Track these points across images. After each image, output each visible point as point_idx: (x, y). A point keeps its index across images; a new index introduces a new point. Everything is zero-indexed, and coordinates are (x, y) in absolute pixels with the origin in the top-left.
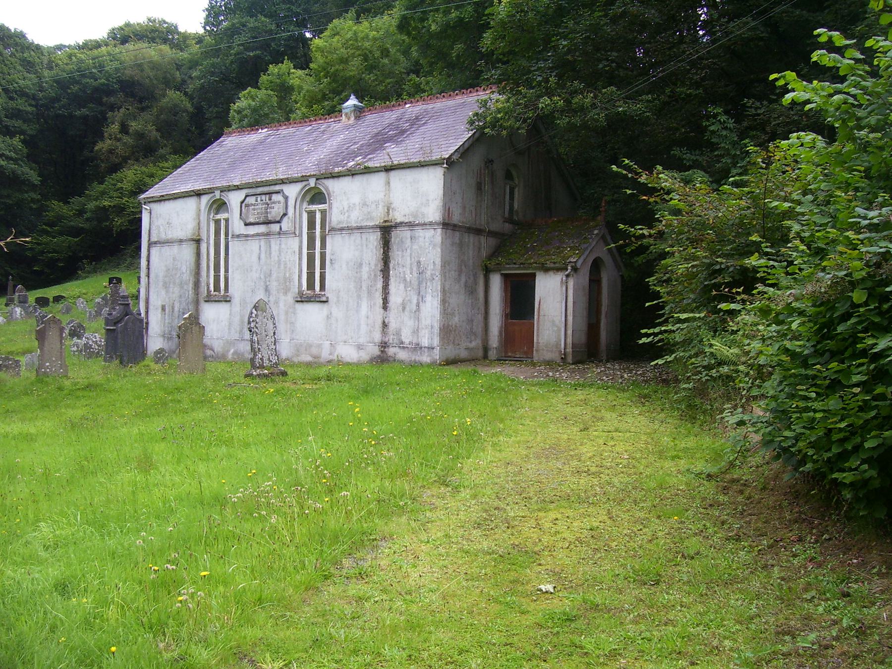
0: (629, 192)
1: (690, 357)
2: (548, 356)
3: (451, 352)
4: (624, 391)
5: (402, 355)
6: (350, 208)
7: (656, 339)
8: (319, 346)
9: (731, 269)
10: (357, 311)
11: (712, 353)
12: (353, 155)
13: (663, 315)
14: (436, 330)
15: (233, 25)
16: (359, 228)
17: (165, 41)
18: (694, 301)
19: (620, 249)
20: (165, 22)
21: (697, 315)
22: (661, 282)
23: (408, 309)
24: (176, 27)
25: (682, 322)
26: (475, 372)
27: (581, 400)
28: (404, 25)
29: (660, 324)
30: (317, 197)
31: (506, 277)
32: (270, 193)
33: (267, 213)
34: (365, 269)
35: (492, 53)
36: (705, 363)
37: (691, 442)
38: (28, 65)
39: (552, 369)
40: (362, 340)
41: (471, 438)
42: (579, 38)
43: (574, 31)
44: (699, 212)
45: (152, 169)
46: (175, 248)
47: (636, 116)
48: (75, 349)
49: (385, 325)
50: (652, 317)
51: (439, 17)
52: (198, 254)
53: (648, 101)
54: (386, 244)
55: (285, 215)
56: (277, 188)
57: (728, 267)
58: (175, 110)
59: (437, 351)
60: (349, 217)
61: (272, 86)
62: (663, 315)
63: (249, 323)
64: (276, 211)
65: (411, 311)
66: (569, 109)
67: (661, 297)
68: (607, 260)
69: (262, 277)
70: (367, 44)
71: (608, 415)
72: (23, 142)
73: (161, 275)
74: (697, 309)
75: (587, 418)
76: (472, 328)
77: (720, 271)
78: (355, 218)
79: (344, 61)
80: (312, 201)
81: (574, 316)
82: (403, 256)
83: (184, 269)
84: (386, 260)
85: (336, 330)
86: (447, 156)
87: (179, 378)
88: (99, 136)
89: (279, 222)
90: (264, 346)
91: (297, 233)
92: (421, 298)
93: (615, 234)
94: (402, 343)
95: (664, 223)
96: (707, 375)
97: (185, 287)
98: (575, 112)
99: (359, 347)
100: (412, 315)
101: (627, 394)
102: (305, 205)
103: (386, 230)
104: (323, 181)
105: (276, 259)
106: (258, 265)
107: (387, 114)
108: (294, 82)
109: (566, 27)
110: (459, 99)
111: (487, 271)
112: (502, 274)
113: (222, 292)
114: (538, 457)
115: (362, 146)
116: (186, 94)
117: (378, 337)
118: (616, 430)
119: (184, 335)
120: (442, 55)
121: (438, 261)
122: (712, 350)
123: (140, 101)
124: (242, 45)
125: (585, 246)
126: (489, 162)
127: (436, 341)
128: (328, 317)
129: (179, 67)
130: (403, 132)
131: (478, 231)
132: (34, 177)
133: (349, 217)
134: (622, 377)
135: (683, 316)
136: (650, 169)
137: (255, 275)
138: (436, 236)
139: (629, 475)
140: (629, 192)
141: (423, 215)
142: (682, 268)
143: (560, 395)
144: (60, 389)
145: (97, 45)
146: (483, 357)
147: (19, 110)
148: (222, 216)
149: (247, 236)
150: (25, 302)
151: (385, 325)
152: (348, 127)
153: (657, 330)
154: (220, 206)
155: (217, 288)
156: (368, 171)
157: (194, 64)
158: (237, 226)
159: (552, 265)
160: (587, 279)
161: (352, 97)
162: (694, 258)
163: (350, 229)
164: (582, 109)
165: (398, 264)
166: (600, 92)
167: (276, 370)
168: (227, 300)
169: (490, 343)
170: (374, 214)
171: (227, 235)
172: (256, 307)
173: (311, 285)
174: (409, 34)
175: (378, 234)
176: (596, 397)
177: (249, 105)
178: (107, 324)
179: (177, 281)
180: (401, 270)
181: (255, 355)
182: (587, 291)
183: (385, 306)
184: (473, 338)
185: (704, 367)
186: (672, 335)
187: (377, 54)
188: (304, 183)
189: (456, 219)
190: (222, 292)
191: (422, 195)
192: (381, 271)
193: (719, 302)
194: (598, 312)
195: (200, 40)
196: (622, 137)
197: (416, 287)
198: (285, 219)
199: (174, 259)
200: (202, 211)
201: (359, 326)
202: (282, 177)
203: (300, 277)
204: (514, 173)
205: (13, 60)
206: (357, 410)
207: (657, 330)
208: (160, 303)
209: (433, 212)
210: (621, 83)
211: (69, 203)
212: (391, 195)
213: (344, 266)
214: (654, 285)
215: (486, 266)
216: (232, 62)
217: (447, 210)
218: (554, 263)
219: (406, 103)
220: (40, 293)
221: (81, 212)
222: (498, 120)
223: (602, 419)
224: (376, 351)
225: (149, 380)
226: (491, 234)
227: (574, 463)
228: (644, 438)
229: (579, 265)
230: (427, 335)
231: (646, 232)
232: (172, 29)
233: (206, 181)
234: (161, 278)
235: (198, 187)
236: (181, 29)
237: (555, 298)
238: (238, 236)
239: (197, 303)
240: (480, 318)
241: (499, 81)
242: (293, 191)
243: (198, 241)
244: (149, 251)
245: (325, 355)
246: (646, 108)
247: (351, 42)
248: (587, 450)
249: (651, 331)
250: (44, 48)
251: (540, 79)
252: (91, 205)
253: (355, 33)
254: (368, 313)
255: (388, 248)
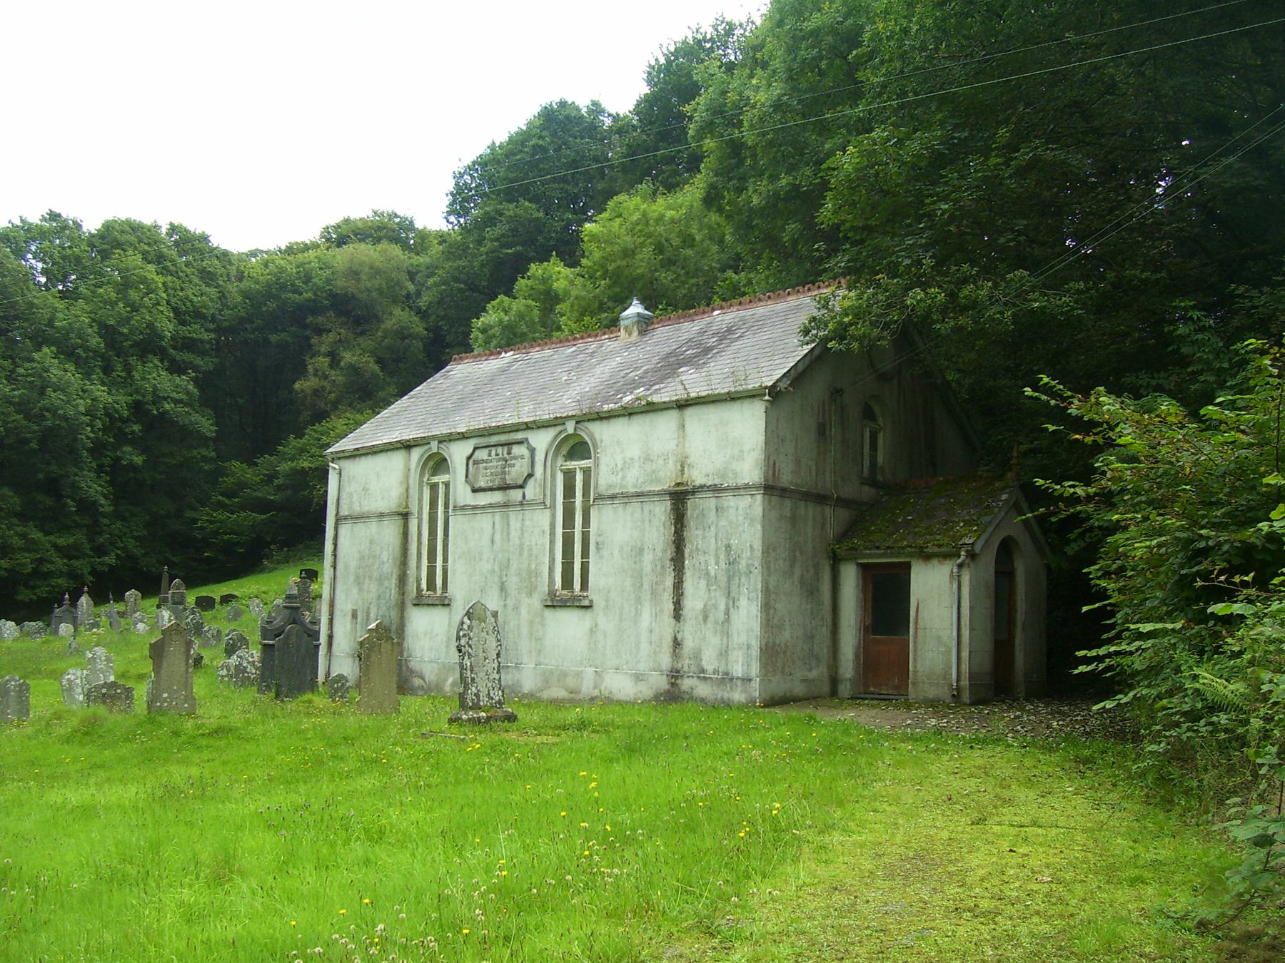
0: (1051, 428)
1: (1159, 697)
2: (932, 692)
3: (780, 686)
4: (1051, 750)
5: (703, 690)
6: (626, 465)
7: (1101, 666)
8: (578, 675)
9: (1226, 548)
10: (636, 619)
11: (1197, 690)
12: (633, 385)
13: (1113, 626)
14: (755, 652)
15: (486, 213)
16: (638, 495)
17: (396, 240)
18: (1163, 602)
19: (1041, 520)
20: (396, 216)
21: (1170, 626)
22: (1106, 574)
23: (711, 618)
24: (411, 223)
25: (1144, 637)
26: (811, 718)
27: (979, 768)
28: (711, 199)
29: (1109, 642)
30: (578, 448)
31: (865, 568)
32: (509, 444)
33: (504, 473)
34: (648, 558)
35: (836, 227)
36: (1186, 708)
37: (1164, 850)
38: (208, 277)
39: (935, 714)
40: (643, 667)
41: (777, 840)
42: (967, 197)
43: (957, 189)
44: (1168, 457)
45: (358, 416)
46: (373, 527)
47: (1062, 314)
48: (224, 672)
49: (677, 644)
50: (1096, 629)
51: (763, 185)
52: (405, 534)
53: (1079, 292)
54: (679, 519)
55: (530, 476)
56: (520, 436)
57: (1219, 545)
58: (403, 334)
59: (756, 684)
60: (623, 478)
61: (533, 294)
62: (1113, 626)
63: (458, 638)
64: (517, 470)
65: (716, 622)
66: (953, 305)
67: (1110, 597)
68: (1023, 539)
69: (497, 569)
70: (661, 229)
71: (1022, 794)
72: (196, 381)
73: (353, 564)
74: (1169, 616)
75: (986, 799)
76: (811, 650)
77: (1205, 552)
78: (633, 480)
79: (628, 253)
80: (571, 456)
81: (971, 629)
82: (704, 538)
83: (385, 556)
84: (679, 543)
85: (605, 649)
86: (770, 384)
87: (352, 721)
88: (301, 371)
89: (521, 487)
90: (482, 674)
91: (548, 503)
92: (732, 601)
93: (1036, 497)
94: (703, 671)
95: (1109, 475)
96: (1189, 729)
97: (386, 584)
98: (964, 309)
99: (638, 678)
100: (719, 628)
101: (1055, 757)
102: (560, 461)
103: (680, 498)
104: (586, 424)
105: (517, 541)
106: (491, 552)
107: (686, 326)
108: (560, 285)
109: (946, 183)
110: (793, 301)
111: (835, 561)
112: (859, 565)
113: (439, 592)
114: (890, 877)
115: (646, 372)
116: (419, 312)
117: (666, 661)
118: (1034, 824)
119: (368, 657)
120: (771, 241)
121: (758, 545)
122: (1197, 685)
123: (358, 321)
124: (497, 240)
125: (988, 518)
126: (836, 392)
127: (755, 670)
128: (593, 631)
129: (412, 276)
130: (707, 350)
131: (820, 499)
132: (205, 424)
133: (623, 478)
134: (1049, 727)
135: (1146, 628)
136: (1086, 393)
137: (486, 566)
138: (756, 504)
139: (1048, 919)
140: (1051, 428)
141: (735, 474)
142: (1140, 548)
143: (946, 758)
144: (176, 734)
145: (306, 248)
146: (828, 693)
147: (193, 340)
148: (440, 479)
149: (475, 507)
150: (182, 602)
151: (677, 644)
152: (628, 347)
153: (1102, 651)
154: (438, 464)
155: (431, 585)
156: (652, 408)
157: (431, 270)
158: (462, 494)
159: (936, 550)
160: (993, 570)
161: (635, 302)
162: (1161, 531)
163: (626, 497)
164: (974, 305)
165: (697, 549)
166: (1004, 279)
167: (500, 713)
168: (445, 603)
169: (841, 671)
170: (662, 474)
171: (446, 506)
172: (468, 614)
173: (567, 582)
174: (720, 210)
175: (667, 504)
176: (1005, 760)
177: (501, 321)
178: (264, 637)
179: (375, 574)
180: (702, 559)
181: (466, 688)
182: (992, 588)
183: (677, 614)
184: (814, 663)
185: (1184, 714)
186: (1126, 661)
187: (676, 241)
188: (559, 428)
189: (786, 479)
190: (439, 592)
191: (733, 445)
192: (672, 559)
193: (1208, 604)
194: (1011, 622)
195: (442, 238)
196: (1036, 342)
197: (723, 584)
198: (531, 483)
199: (372, 542)
200: (412, 471)
201: (638, 644)
202: (526, 420)
203: (551, 569)
204: (877, 409)
205: (189, 271)
206: (593, 784)
207: (1102, 651)
208: (349, 607)
209: (750, 470)
210: (1033, 265)
211: (256, 464)
212: (687, 445)
213: (616, 553)
214: (1099, 578)
215: (834, 552)
216: (482, 265)
217: (771, 465)
218: (940, 546)
219: (713, 310)
220: (204, 592)
221: (270, 478)
222: (845, 328)
223: (1009, 802)
224: (662, 683)
225: (306, 724)
226: (842, 502)
227: (953, 890)
228: (1081, 838)
229: (977, 548)
230: (740, 660)
231: (1080, 491)
232: (408, 225)
233: (419, 427)
234: (352, 569)
235: (407, 435)
236: (419, 225)
237: (940, 599)
238: (463, 508)
239: (402, 607)
240: (825, 632)
241: (847, 272)
242: (542, 441)
243: (405, 516)
244: (336, 529)
245: (587, 688)
246: (1076, 302)
247: (639, 228)
248: (979, 862)
249: (1093, 653)
250: (233, 254)
251: (908, 262)
252: (285, 467)
253: (644, 214)
254: (652, 623)
255: (683, 525)
